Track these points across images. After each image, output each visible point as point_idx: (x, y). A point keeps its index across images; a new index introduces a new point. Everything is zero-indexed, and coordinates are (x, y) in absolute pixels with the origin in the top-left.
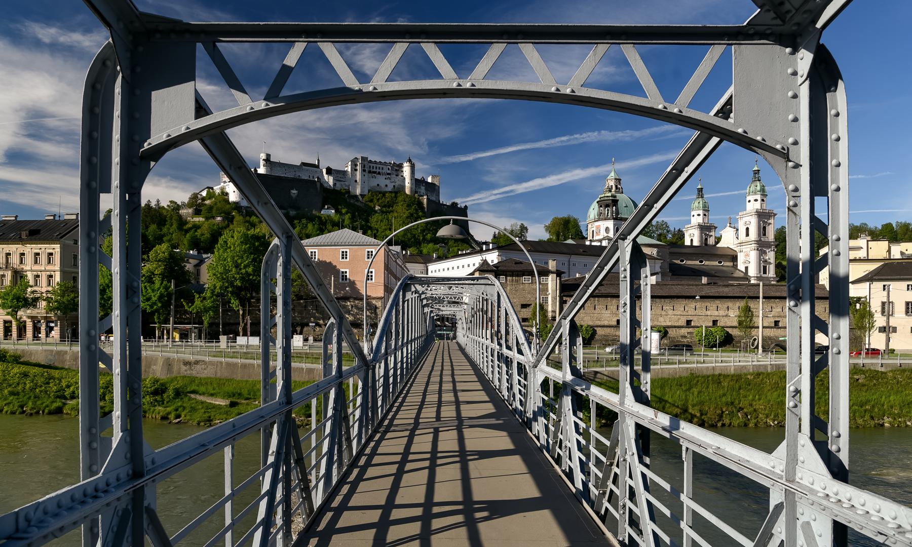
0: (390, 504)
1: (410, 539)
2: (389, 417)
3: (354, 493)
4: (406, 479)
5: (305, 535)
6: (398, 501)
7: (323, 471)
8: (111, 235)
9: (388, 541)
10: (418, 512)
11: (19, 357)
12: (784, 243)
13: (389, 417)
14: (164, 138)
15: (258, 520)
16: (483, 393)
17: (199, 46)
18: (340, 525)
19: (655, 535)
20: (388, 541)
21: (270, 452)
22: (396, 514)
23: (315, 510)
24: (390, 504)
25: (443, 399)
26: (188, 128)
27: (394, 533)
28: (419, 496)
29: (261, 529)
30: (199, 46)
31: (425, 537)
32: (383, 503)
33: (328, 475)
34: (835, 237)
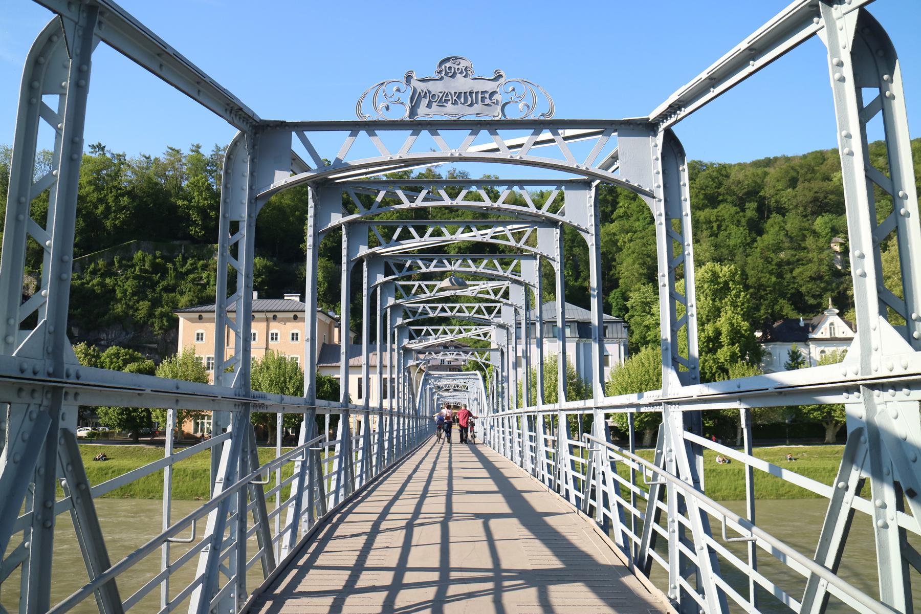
0: (401, 568)
1: (421, 606)
2: (384, 476)
3: (361, 551)
4: (380, 541)
5: (257, 603)
6: (369, 563)
7: (289, 520)
8: (620, 394)
9: (396, 607)
10: (435, 576)
11: (556, 428)
12: (743, 481)
13: (384, 476)
14: (283, 183)
15: (197, 577)
16: (490, 481)
17: (294, 133)
18: (300, 588)
19: (720, 591)
20: (396, 607)
21: (218, 480)
22: (409, 578)
23: (277, 566)
24: (401, 568)
25: (454, 475)
26: (286, 182)
27: (404, 599)
28: (392, 559)
29: (200, 587)
30: (294, 133)
31: (437, 605)
32: (394, 564)
33: (294, 526)
34: (880, 523)
